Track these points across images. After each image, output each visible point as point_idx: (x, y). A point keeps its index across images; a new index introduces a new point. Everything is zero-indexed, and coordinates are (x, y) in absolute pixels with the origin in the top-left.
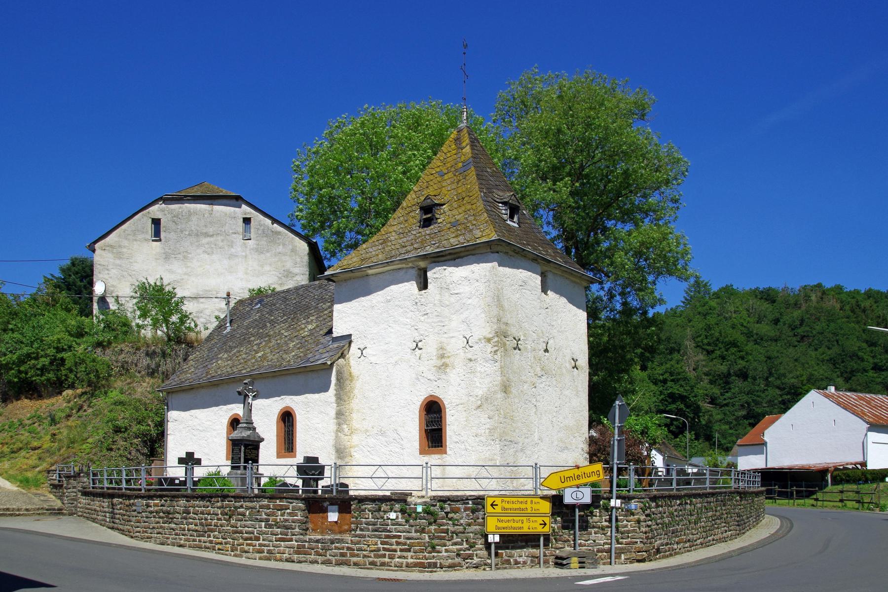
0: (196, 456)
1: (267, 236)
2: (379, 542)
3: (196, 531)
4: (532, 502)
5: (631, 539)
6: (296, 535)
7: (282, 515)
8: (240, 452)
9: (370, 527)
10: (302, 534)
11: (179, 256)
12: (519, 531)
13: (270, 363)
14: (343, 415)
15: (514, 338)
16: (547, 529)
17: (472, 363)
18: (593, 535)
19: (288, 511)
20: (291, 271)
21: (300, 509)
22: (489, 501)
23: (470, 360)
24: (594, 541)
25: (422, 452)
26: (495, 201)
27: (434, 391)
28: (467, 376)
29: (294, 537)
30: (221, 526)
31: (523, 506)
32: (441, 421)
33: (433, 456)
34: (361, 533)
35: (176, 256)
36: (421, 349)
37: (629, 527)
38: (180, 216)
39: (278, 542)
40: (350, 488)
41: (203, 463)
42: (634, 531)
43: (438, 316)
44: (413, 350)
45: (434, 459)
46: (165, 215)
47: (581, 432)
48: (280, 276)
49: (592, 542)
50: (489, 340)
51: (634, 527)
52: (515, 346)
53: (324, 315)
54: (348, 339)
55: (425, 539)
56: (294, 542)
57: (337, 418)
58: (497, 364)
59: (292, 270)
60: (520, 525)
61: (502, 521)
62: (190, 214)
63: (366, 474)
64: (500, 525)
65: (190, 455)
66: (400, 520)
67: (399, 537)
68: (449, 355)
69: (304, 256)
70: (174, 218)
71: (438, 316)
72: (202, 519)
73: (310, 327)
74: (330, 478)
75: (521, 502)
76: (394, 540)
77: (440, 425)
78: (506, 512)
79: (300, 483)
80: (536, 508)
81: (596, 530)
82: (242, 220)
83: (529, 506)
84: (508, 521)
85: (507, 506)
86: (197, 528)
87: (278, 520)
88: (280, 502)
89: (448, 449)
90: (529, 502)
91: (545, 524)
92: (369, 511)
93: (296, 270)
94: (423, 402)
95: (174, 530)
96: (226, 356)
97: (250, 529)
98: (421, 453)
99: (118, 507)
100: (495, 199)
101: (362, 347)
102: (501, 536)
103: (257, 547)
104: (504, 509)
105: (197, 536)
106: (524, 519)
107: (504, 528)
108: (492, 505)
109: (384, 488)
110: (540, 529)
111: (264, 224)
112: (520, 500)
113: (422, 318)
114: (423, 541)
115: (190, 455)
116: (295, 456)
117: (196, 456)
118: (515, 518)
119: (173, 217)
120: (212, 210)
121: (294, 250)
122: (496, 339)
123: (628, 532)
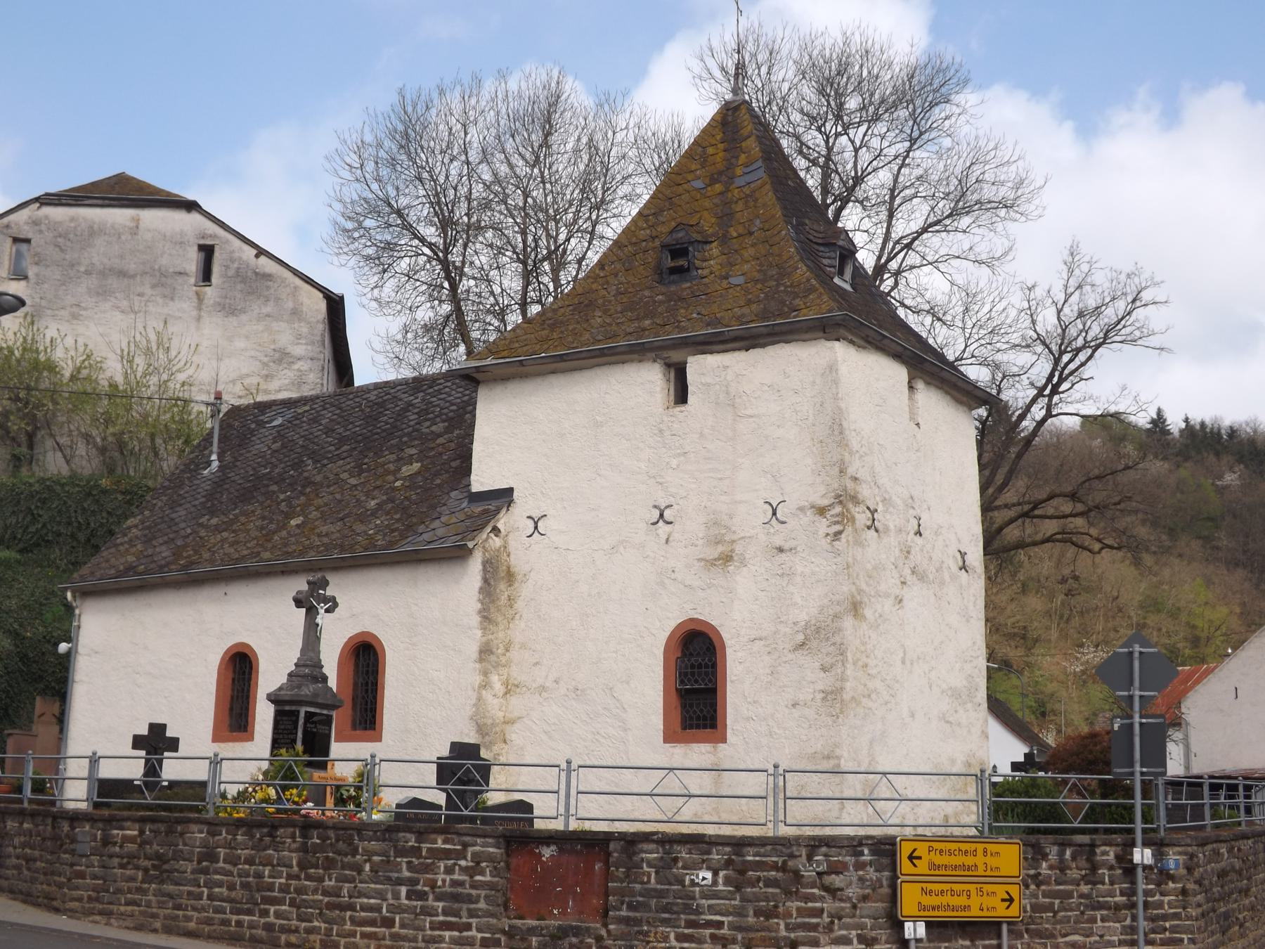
0: (169, 734)
1: (243, 281)
2: (672, 936)
3: (231, 901)
4: (985, 851)
5: (1171, 932)
6: (478, 917)
7: (449, 871)
8: (296, 728)
9: (653, 902)
10: (492, 915)
11: (62, 312)
12: (963, 914)
13: (326, 540)
14: (492, 653)
15: (868, 508)
16: (1014, 910)
17: (783, 555)
18: (1100, 923)
19: (463, 863)
20: (287, 351)
21: (491, 858)
22: (906, 849)
23: (781, 550)
24: (1101, 936)
25: (670, 737)
26: (811, 241)
27: (699, 611)
28: (773, 581)
29: (474, 921)
30: (299, 891)
31: (969, 861)
32: (714, 674)
33: (695, 746)
34: (631, 914)
35: (56, 312)
36: (671, 523)
37: (1166, 907)
38: (71, 236)
39: (437, 933)
40: (536, 812)
41: (183, 749)
42: (1176, 916)
43: (709, 459)
44: (654, 524)
45: (698, 753)
46: (41, 232)
47: (975, 700)
48: (266, 360)
49: (1097, 938)
50: (821, 511)
51: (1176, 908)
52: (869, 523)
53: (439, 445)
54: (504, 496)
55: (777, 930)
56: (473, 933)
57: (481, 660)
58: (839, 559)
59: (290, 349)
60: (962, 901)
61: (931, 891)
62: (93, 232)
63: (539, 782)
64: (929, 901)
65: (157, 730)
66: (721, 888)
67: (719, 925)
68: (735, 537)
69: (318, 322)
70: (59, 240)
71: (709, 459)
72: (248, 876)
73: (407, 470)
74: (785, 798)
75: (966, 852)
76: (708, 932)
77: (710, 681)
78: (937, 872)
79: (440, 798)
80: (994, 866)
81: (1105, 912)
82: (196, 248)
83: (980, 860)
84: (942, 892)
85: (939, 860)
86: (233, 894)
87: (440, 883)
88: (445, 842)
89: (729, 732)
90: (980, 852)
91: (1011, 900)
92: (650, 865)
93: (299, 350)
94: (673, 633)
95: (170, 896)
96: (214, 521)
97: (372, 901)
98: (666, 741)
99: (16, 841)
100: (812, 238)
101: (536, 515)
102: (929, 925)
103: (388, 943)
104: (933, 866)
105: (231, 913)
106: (972, 888)
107: (934, 908)
108: (911, 858)
109: (677, 818)
110: (1001, 911)
111: (240, 258)
112: (964, 847)
113: (674, 463)
114: (774, 934)
115: (157, 730)
116: (251, 738)
117: (169, 734)
118: (955, 887)
119: (56, 237)
120: (137, 227)
121: (296, 313)
122: (838, 509)
123: (1165, 917)
